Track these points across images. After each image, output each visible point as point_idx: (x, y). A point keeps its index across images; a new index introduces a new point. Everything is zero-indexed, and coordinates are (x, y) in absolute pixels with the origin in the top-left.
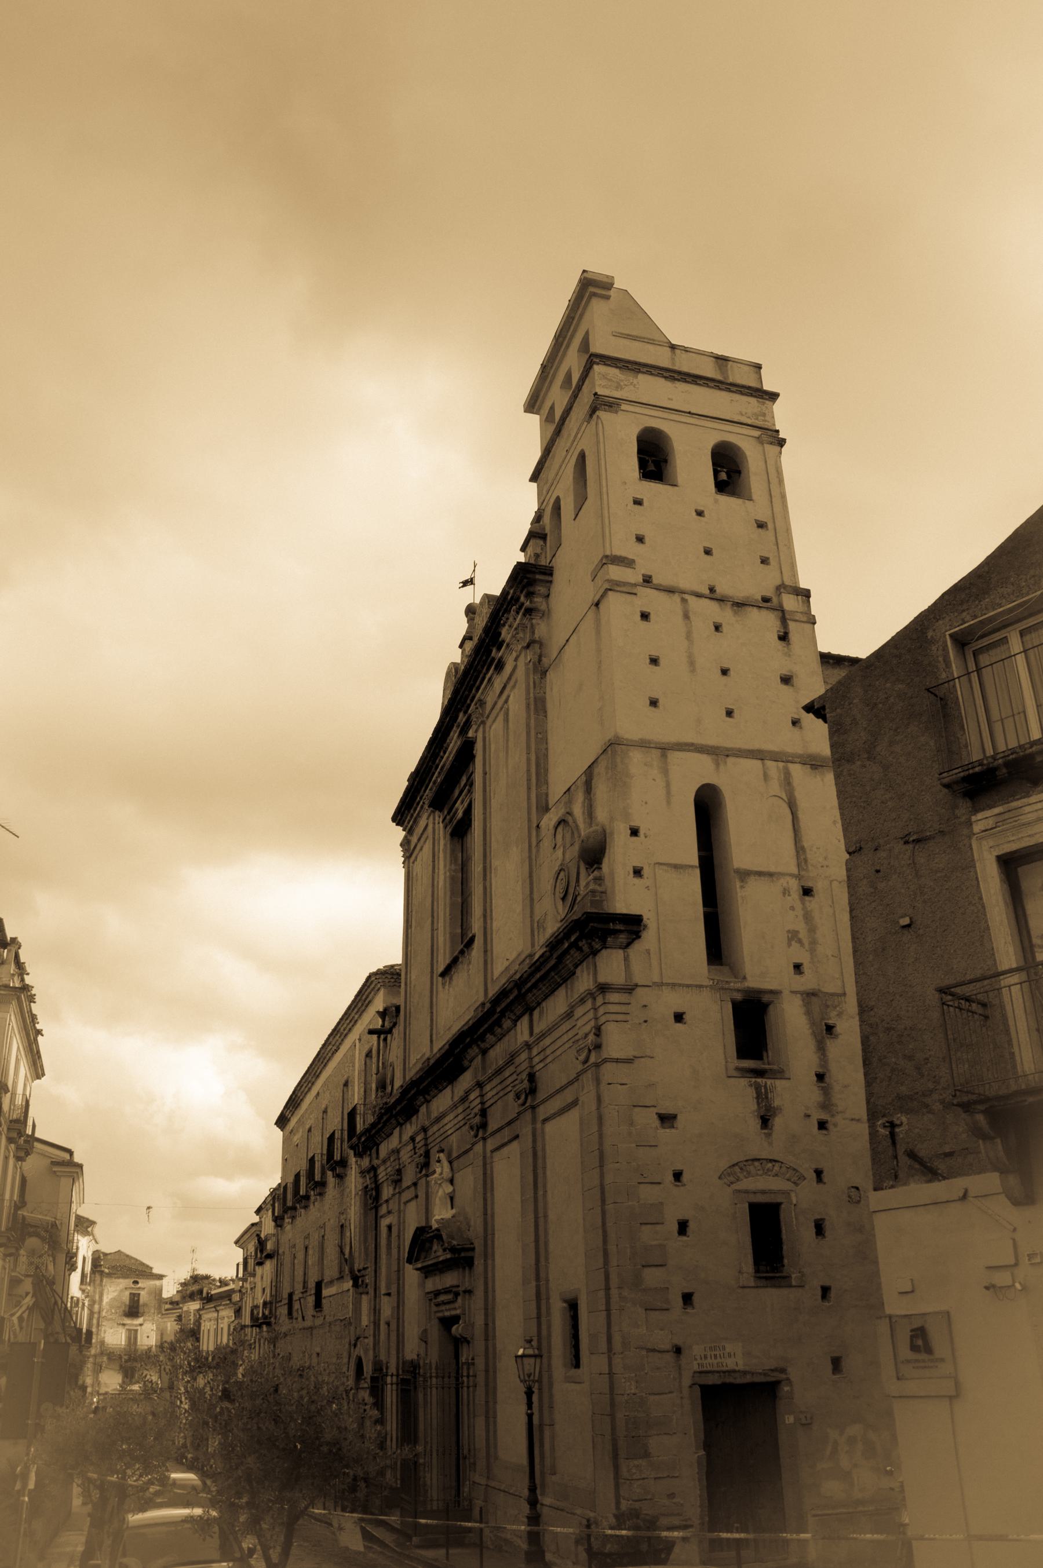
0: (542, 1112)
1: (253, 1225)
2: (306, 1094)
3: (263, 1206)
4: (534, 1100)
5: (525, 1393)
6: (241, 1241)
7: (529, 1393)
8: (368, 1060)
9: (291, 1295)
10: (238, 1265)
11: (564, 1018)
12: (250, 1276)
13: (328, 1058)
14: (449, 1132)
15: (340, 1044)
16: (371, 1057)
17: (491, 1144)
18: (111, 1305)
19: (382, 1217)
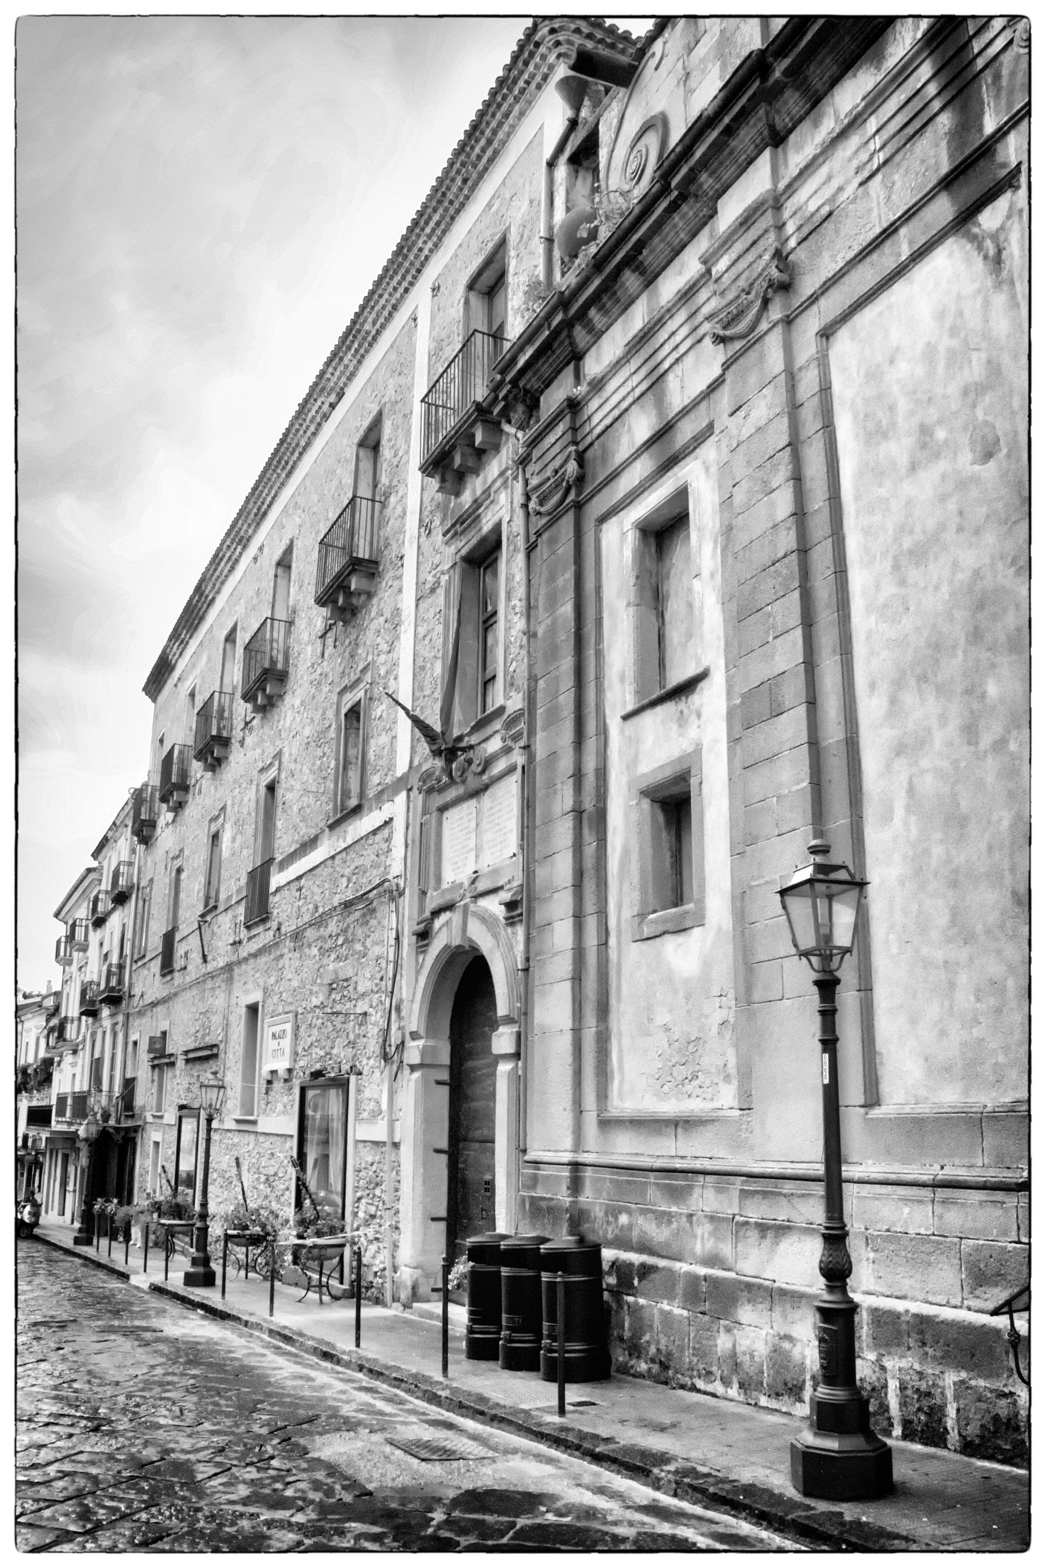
0: (598, 506)
1: (89, 871)
2: (227, 576)
3: (110, 835)
4: (579, 493)
5: (817, 983)
6: (63, 913)
7: (827, 986)
8: (228, 646)
9: (169, 939)
10: (59, 942)
11: (634, 346)
12: (79, 950)
13: (267, 502)
14: (666, 365)
15: (314, 434)
16: (234, 642)
17: (811, 323)
18: (534, 1227)
19: (800, 369)
